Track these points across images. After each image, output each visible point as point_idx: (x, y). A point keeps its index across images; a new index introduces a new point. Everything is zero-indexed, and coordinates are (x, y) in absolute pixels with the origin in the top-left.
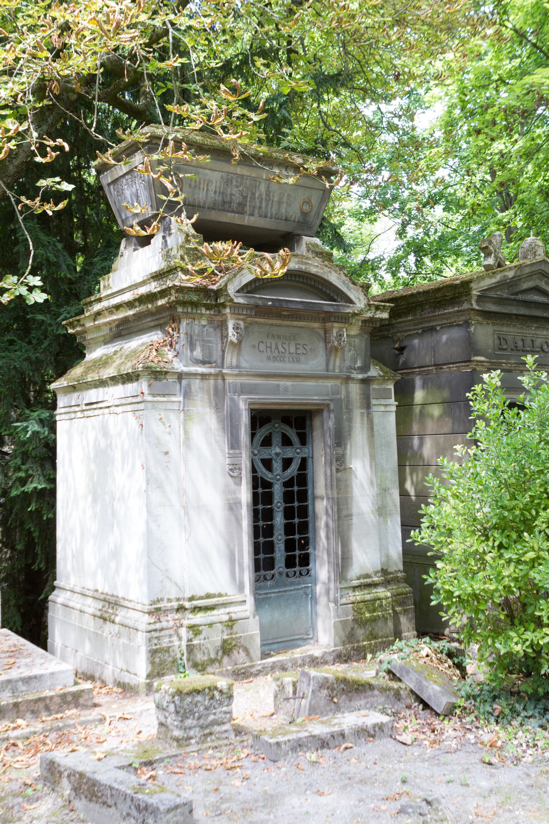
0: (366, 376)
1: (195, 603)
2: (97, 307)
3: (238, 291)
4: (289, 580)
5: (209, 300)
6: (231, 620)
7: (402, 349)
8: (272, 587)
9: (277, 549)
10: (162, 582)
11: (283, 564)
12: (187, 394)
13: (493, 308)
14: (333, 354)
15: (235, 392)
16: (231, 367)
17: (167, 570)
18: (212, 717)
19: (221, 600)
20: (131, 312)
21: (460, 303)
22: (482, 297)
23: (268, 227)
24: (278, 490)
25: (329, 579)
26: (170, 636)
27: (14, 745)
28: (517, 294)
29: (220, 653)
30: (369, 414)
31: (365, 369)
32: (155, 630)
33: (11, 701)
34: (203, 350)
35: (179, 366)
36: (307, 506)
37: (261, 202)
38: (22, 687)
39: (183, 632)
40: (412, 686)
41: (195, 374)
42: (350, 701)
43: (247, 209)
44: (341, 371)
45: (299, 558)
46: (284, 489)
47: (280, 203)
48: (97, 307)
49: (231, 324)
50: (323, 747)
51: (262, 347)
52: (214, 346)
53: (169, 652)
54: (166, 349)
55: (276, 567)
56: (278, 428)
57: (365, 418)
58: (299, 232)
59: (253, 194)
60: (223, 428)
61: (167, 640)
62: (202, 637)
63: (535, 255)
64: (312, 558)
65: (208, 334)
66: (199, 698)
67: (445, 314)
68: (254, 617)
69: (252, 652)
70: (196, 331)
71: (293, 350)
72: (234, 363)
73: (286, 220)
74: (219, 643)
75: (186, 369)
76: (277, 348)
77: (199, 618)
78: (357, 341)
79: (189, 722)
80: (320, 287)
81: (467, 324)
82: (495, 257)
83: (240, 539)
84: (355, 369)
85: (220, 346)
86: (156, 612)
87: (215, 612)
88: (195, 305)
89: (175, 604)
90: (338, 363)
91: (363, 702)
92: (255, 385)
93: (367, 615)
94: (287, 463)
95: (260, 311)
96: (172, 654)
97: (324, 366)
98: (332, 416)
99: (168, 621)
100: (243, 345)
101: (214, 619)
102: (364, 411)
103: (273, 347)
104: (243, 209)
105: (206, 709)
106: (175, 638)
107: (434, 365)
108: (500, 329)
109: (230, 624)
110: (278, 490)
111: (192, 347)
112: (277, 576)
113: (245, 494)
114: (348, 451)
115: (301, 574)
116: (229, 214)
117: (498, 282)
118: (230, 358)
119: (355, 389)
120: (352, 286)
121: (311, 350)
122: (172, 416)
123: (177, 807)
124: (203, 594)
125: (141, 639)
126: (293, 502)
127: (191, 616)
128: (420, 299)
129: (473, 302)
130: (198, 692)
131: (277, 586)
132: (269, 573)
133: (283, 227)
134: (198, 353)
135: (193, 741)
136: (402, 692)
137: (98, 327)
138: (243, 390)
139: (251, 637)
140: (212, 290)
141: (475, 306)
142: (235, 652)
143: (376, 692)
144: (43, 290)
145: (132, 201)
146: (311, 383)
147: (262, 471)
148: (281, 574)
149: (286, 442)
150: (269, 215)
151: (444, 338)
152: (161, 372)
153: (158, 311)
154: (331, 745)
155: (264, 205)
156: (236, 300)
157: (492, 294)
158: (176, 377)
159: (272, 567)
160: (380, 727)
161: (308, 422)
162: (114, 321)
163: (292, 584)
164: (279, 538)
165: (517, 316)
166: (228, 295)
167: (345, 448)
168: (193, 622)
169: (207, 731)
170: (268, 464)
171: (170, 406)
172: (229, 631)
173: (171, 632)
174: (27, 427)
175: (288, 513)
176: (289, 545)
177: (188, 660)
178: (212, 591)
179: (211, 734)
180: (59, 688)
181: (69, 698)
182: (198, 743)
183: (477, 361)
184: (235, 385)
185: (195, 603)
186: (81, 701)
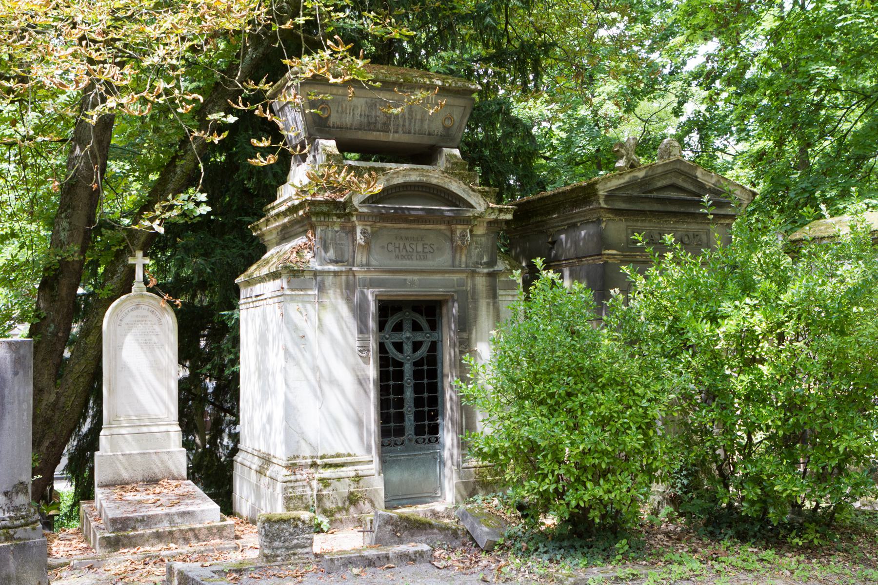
0: (491, 270)
1: (326, 460)
2: (273, 212)
3: (363, 202)
4: (419, 446)
5: (338, 210)
6: (357, 476)
7: (553, 243)
8: (402, 451)
9: (407, 419)
11: (412, 432)
12: (322, 288)
13: (623, 206)
14: (458, 251)
15: (364, 286)
16: (362, 265)
17: (303, 433)
18: (295, 541)
19: (349, 459)
20: (286, 220)
21: (590, 203)
22: (611, 196)
23: (412, 141)
24: (408, 369)
25: (452, 445)
26: (304, 486)
27: (162, 560)
28: (651, 192)
30: (494, 303)
31: (492, 263)
32: (290, 481)
33: (167, 529)
34: (335, 252)
35: (315, 265)
36: (436, 383)
37: (404, 121)
38: (178, 520)
39: (314, 483)
40: (468, 527)
41: (328, 272)
42: (412, 536)
43: (392, 127)
44: (466, 266)
45: (429, 429)
46: (413, 368)
47: (422, 120)
48: (273, 212)
49: (358, 231)
50: (369, 565)
51: (391, 247)
52: (346, 248)
53: (302, 499)
54: (306, 251)
55: (406, 434)
56: (408, 316)
57: (491, 307)
58: (442, 144)
60: (354, 316)
61: (301, 489)
62: (331, 488)
63: (670, 155)
64: (440, 428)
65: (340, 239)
66: (285, 526)
67: (582, 212)
68: (379, 474)
69: (376, 504)
70: (330, 236)
71: (420, 249)
72: (364, 261)
73: (429, 134)
74: (346, 495)
75: (319, 268)
76: (405, 248)
77: (327, 473)
79: (276, 544)
80: (443, 195)
81: (599, 221)
82: (627, 158)
83: (368, 409)
84: (481, 264)
85: (351, 248)
86: (292, 467)
87: (344, 469)
88: (327, 215)
89: (309, 461)
90: (463, 259)
91: (423, 538)
92: (383, 279)
93: (489, 478)
94: (416, 346)
95: (383, 217)
96: (305, 501)
97: (450, 262)
98: (456, 305)
99: (302, 475)
100: (373, 246)
101: (343, 475)
102: (490, 301)
103: (401, 247)
104: (388, 127)
105: (291, 534)
106: (308, 489)
107: (577, 258)
108: (635, 224)
110: (408, 369)
111: (326, 250)
112: (407, 442)
113: (372, 371)
114: (473, 336)
115: (430, 441)
117: (628, 182)
118: (360, 258)
119: (481, 282)
122: (309, 306)
124: (333, 454)
125: (279, 486)
126: (423, 379)
127: (322, 471)
128: (561, 199)
129: (601, 201)
130: (285, 521)
131: (407, 451)
132: (399, 439)
133: (426, 141)
134: (331, 254)
135: (279, 559)
136: (459, 532)
137: (270, 231)
138: (372, 284)
139: (376, 490)
140: (340, 202)
141: (603, 205)
142: (361, 503)
143: (436, 531)
144: (208, 203)
145: (292, 124)
146: (437, 277)
147: (393, 352)
148: (410, 440)
149: (416, 327)
150: (413, 131)
151: (583, 233)
152: (298, 271)
153: (313, 215)
156: (360, 210)
157: (620, 193)
158: (312, 274)
159: (403, 434)
160: (421, 554)
161: (438, 311)
162: (279, 226)
163: (421, 449)
164: (409, 410)
165: (653, 213)
166: (353, 206)
167: (470, 333)
168: (322, 476)
170: (399, 346)
171: (306, 298)
172: (356, 485)
173: (305, 483)
174: (232, 314)
175: (417, 389)
176: (418, 416)
177: (318, 507)
178: (342, 451)
179: (294, 554)
180: (207, 522)
181: (215, 531)
182: (283, 560)
183: (608, 254)
184: (365, 280)
185: (326, 460)
186: (225, 534)
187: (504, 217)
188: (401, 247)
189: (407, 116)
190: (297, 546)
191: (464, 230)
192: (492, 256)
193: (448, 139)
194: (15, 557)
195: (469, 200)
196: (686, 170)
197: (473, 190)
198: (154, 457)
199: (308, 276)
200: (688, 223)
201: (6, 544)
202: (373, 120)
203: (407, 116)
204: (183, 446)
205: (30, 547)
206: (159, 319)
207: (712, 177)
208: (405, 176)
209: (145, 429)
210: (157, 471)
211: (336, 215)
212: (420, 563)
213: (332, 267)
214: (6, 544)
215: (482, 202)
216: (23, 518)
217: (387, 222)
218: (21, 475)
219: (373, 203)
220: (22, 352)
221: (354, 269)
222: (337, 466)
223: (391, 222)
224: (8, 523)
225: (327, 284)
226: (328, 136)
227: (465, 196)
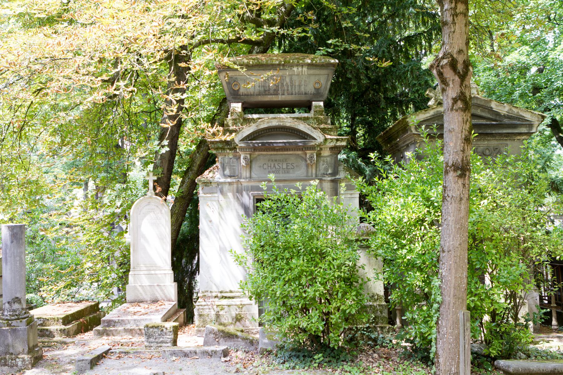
0: (333, 178)
10: (207, 283)
14: (310, 167)
18: (161, 339)
23: (294, 99)
29: (235, 320)
41: (225, 183)
43: (280, 92)
47: (300, 86)
50: (185, 356)
52: (237, 168)
59: (282, 84)
66: (156, 330)
71: (285, 166)
74: (234, 315)
76: (274, 166)
77: (225, 302)
78: (329, 159)
79: (151, 340)
82: (435, 99)
84: (327, 174)
87: (234, 300)
97: (305, 174)
100: (254, 166)
103: (272, 166)
109: (241, 306)
116: (269, 96)
120: (314, 130)
121: (297, 166)
123: (83, 360)
133: (303, 98)
150: (294, 93)
154: (189, 356)
155: (290, 88)
166: (235, 143)
168: (219, 303)
169: (159, 345)
171: (213, 198)
179: (161, 346)
184: (248, 187)
187: (340, 144)
188: (272, 166)
189: (289, 84)
190: (162, 342)
191: (312, 154)
192: (334, 169)
193: (317, 95)
194: (11, 335)
195: (312, 134)
196: (482, 103)
197: (315, 128)
198: (157, 288)
199: (214, 185)
200: (489, 140)
201: (7, 328)
202: (267, 89)
203: (289, 84)
204: (175, 281)
205: (18, 330)
206: (161, 211)
207: (505, 107)
208: (268, 123)
209: (153, 272)
210: (158, 295)
211: (229, 149)
212: (215, 357)
213: (229, 180)
214: (7, 328)
215: (321, 136)
216: (17, 315)
217: (262, 151)
218: (16, 294)
219: (250, 140)
220: (15, 231)
221: (242, 180)
222: (229, 298)
223: (264, 151)
224: (8, 318)
225: (224, 189)
226: (237, 100)
227: (309, 132)
